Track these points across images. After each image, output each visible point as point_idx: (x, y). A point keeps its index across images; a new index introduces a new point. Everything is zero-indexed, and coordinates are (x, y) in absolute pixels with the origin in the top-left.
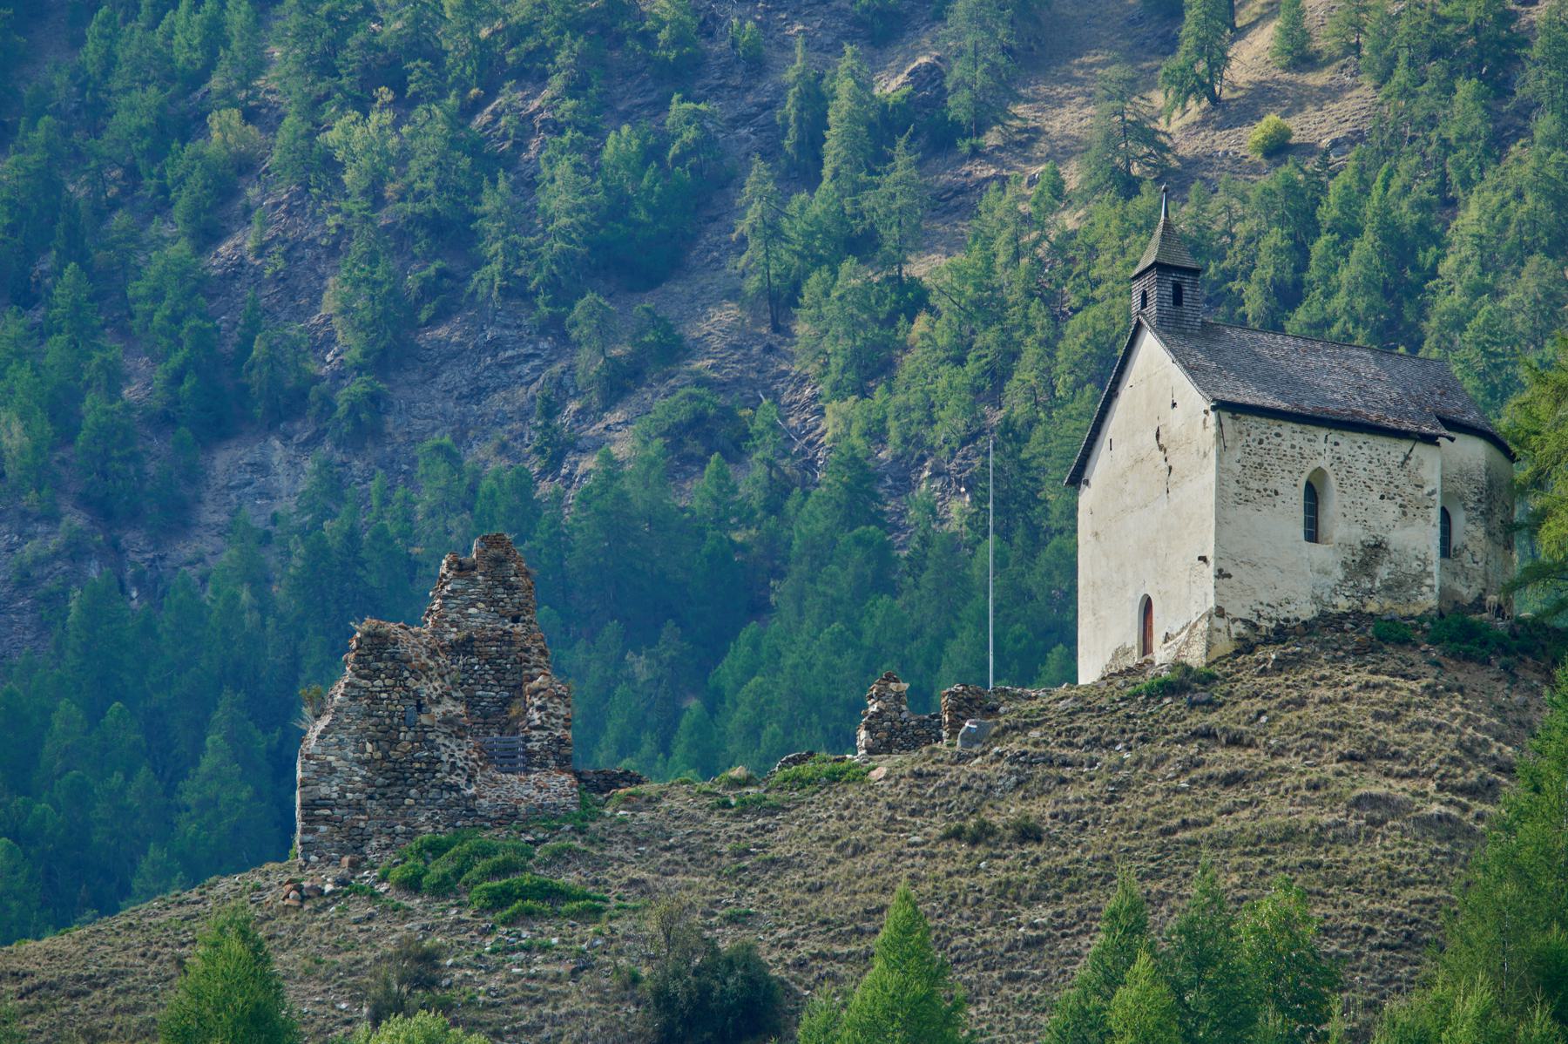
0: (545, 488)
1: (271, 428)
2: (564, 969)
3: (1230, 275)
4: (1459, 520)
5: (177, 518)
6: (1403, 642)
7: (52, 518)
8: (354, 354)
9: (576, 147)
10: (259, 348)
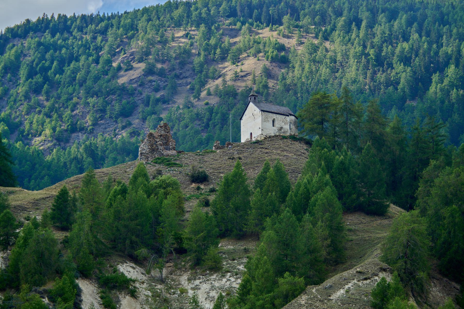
0: (114, 139)
2: (178, 173)
3: (202, 117)
4: (291, 125)
6: (286, 138)
8: (90, 124)
9: (119, 102)
10: (78, 123)
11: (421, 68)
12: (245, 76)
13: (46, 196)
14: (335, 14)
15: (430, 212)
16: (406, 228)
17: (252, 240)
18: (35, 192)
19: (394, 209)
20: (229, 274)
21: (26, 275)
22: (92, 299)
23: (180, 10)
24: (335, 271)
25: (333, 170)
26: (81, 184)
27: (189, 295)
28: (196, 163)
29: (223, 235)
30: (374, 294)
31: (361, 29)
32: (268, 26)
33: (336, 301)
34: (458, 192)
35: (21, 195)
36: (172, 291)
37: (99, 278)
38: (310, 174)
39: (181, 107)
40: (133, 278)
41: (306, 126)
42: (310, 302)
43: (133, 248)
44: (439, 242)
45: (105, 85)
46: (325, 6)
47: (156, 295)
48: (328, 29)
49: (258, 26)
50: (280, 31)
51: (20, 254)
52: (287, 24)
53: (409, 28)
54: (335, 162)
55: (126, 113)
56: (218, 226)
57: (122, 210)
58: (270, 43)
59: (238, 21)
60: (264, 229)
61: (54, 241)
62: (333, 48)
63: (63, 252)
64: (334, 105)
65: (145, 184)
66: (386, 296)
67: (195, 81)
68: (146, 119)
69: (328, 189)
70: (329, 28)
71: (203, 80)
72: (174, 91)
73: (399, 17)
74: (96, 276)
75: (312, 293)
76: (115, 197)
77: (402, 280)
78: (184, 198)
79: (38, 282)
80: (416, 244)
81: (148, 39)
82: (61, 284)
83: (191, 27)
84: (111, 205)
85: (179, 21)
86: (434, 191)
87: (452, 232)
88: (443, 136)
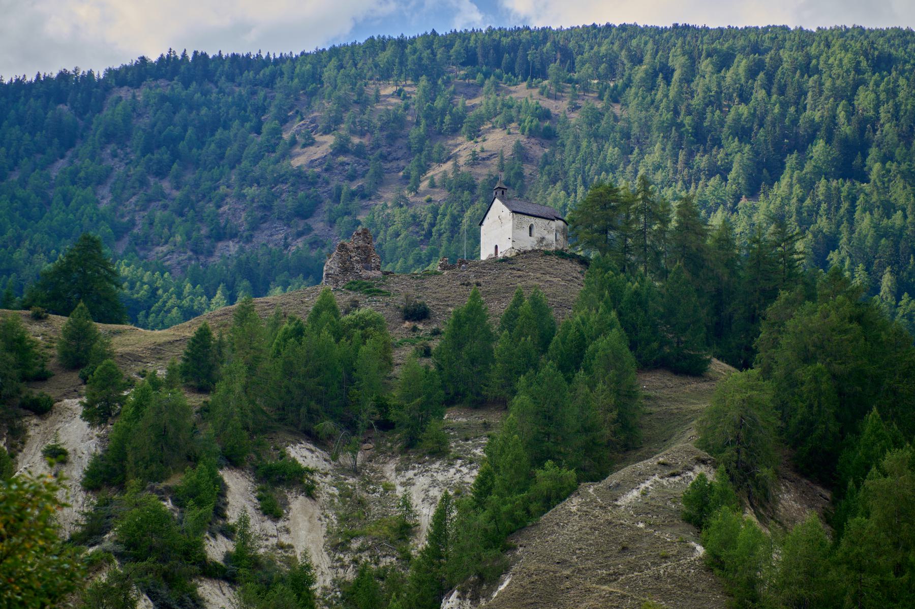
0: (285, 252)
1: (230, 239)
5: (210, 253)
7: (185, 253)
11: (767, 146)
12: (488, 158)
13: (174, 338)
14: (632, 61)
15: (778, 373)
16: (738, 397)
17: (496, 409)
18: (157, 332)
19: (718, 366)
20: (459, 461)
21: (136, 463)
22: (244, 501)
23: (388, 53)
24: (625, 462)
25: (622, 305)
26: (231, 320)
27: (397, 494)
28: (411, 291)
29: (451, 401)
30: (687, 500)
31: (672, 83)
32: (525, 80)
33: (626, 509)
34: (826, 342)
35: (133, 337)
36: (371, 487)
37: (257, 468)
38: (586, 310)
39: (389, 204)
40: (310, 467)
41: (582, 234)
42: (585, 508)
43: (311, 419)
44: (793, 420)
45: (271, 167)
46: (616, 47)
47: (345, 494)
48: (619, 85)
49: (509, 80)
50: (544, 88)
51: (129, 430)
52: (554, 77)
53: (750, 81)
54: (627, 292)
55: (304, 212)
56: (443, 387)
57: (295, 362)
58: (528, 107)
59: (478, 71)
60: (514, 393)
61: (185, 409)
62: (625, 116)
63: (199, 427)
64: (626, 203)
65: (333, 322)
66: (706, 504)
67: (412, 166)
68: (335, 222)
69: (615, 333)
70: (620, 83)
71: (423, 163)
72: (380, 180)
73: (735, 64)
74: (252, 465)
75: (588, 494)
76: (285, 340)
77: (732, 479)
78: (393, 344)
79: (155, 475)
80: (754, 423)
81: (339, 98)
82: (194, 477)
83: (406, 80)
84: (279, 352)
85: (388, 70)
86: (784, 341)
87: (816, 404)
88: (801, 253)
